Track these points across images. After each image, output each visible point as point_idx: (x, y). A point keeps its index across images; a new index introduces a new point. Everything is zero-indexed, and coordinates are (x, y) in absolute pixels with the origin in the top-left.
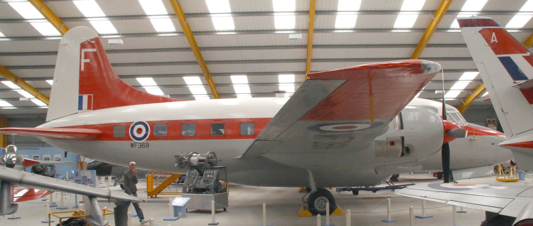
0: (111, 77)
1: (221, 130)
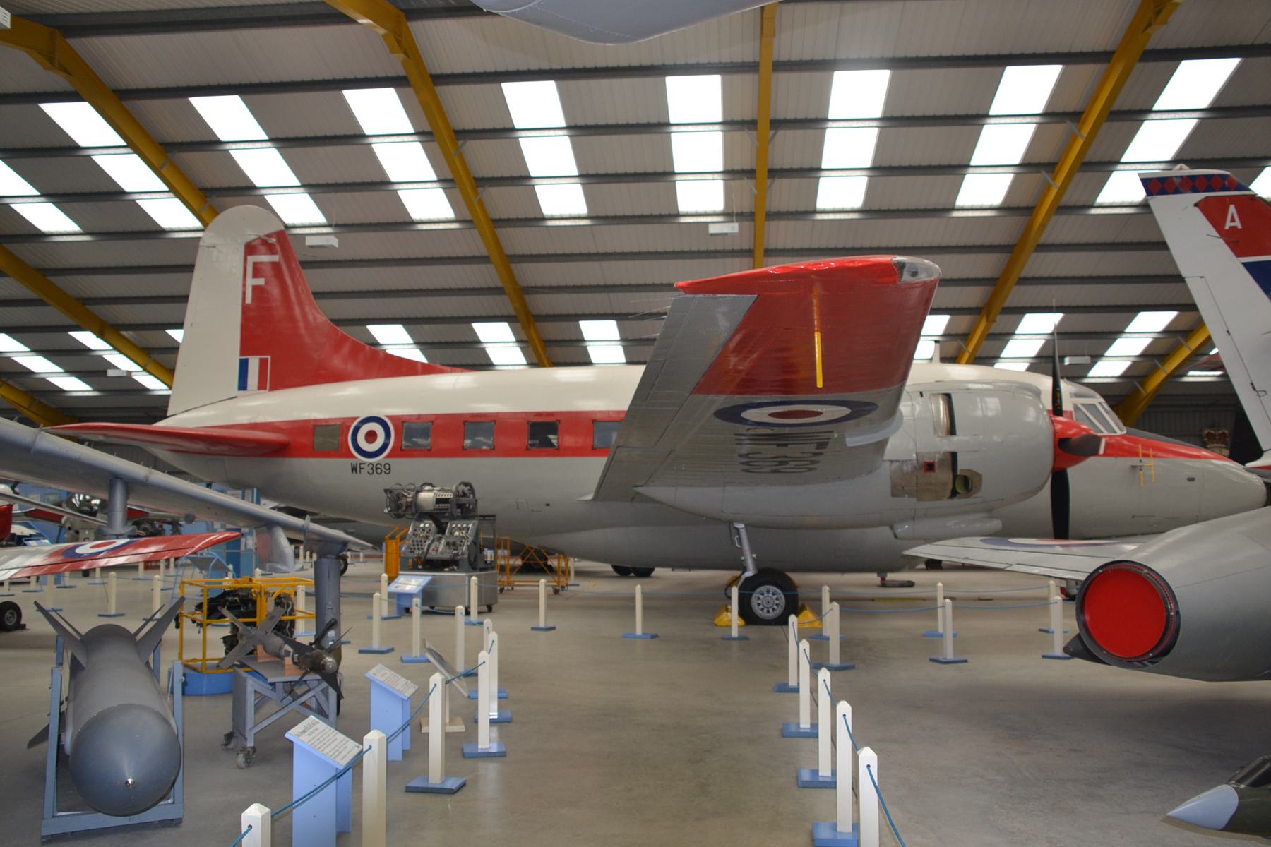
0: (310, 317)
1: (551, 437)
